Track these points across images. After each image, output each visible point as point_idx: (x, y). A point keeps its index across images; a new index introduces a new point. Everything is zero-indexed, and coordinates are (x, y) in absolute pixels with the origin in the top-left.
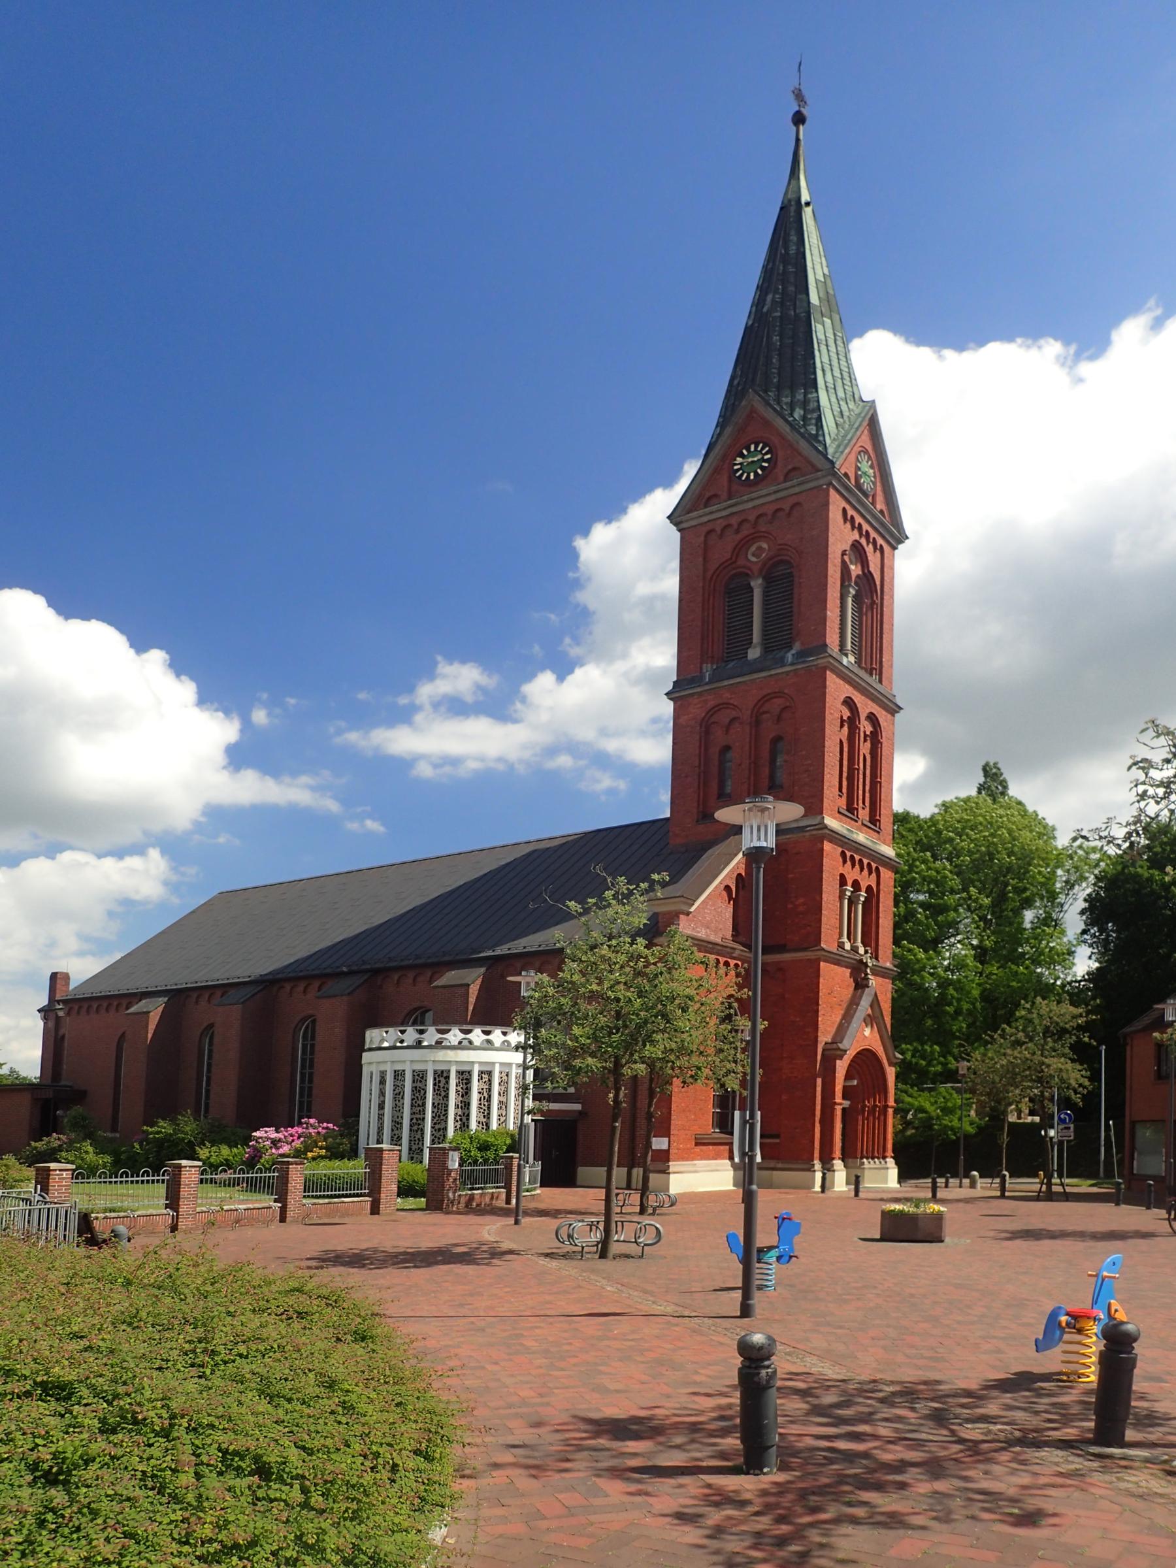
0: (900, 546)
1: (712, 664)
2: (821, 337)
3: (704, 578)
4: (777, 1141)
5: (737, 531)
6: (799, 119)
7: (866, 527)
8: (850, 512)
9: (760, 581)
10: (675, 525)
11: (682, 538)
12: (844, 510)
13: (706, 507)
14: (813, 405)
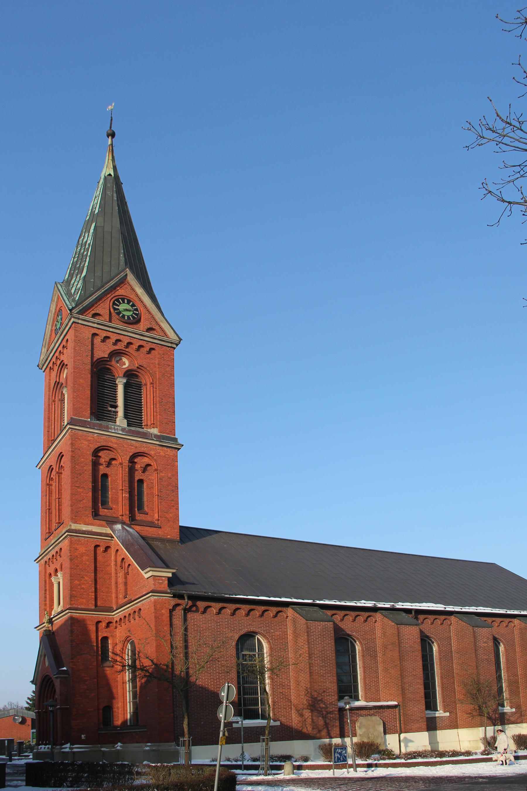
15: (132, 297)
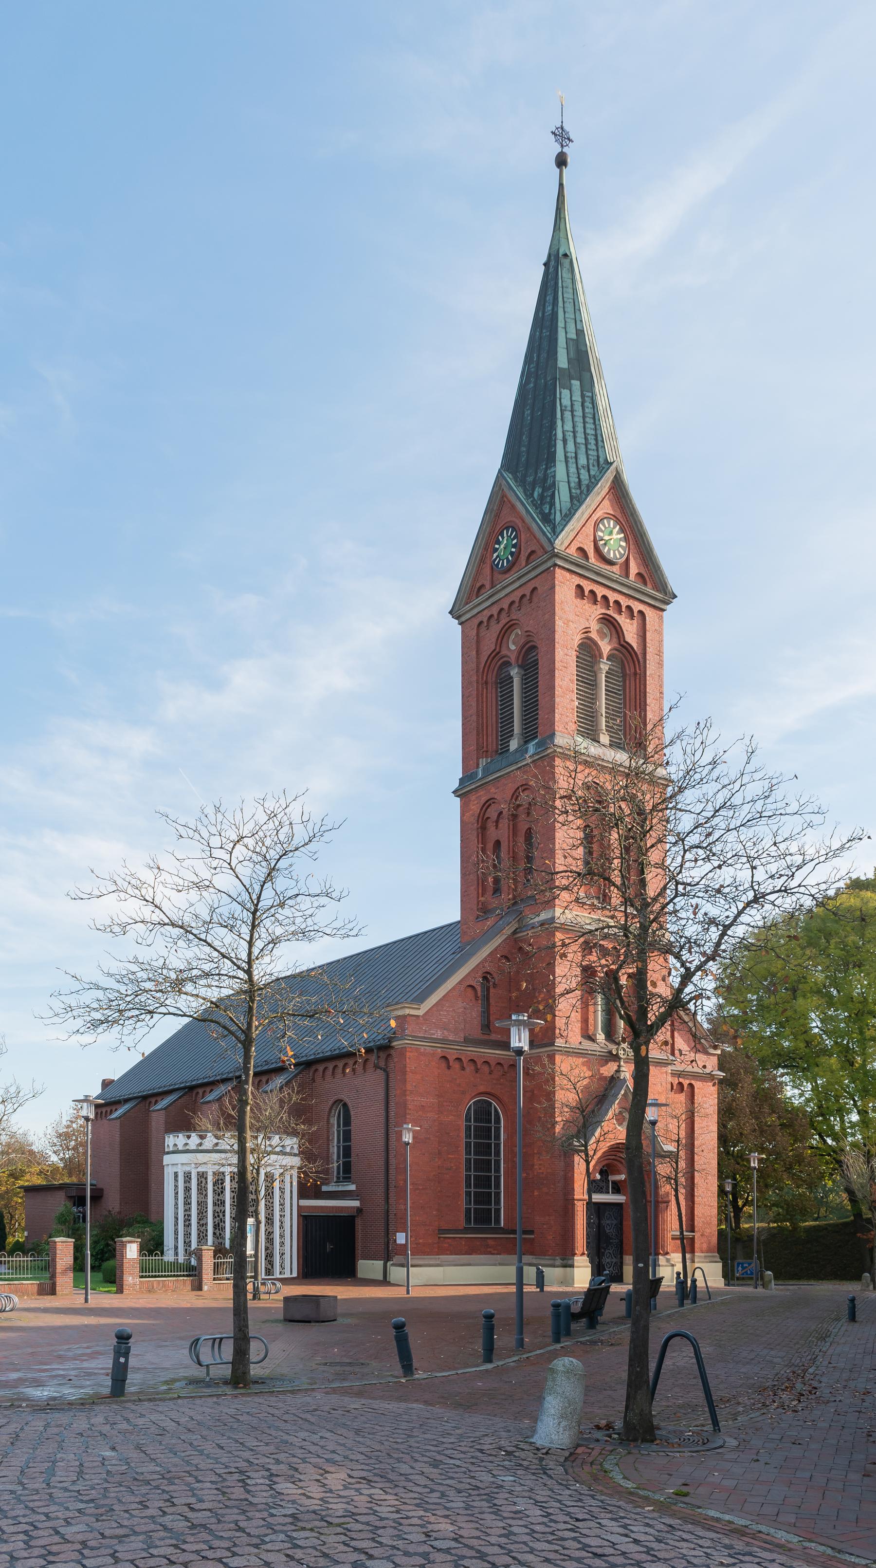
0: (668, 607)
1: (487, 757)
2: (566, 402)
3: (477, 671)
4: (532, 1236)
6: (561, 161)
7: (612, 597)
8: (587, 586)
9: (516, 670)
10: (457, 618)
11: (463, 631)
12: (579, 587)
13: (477, 597)
14: (550, 481)
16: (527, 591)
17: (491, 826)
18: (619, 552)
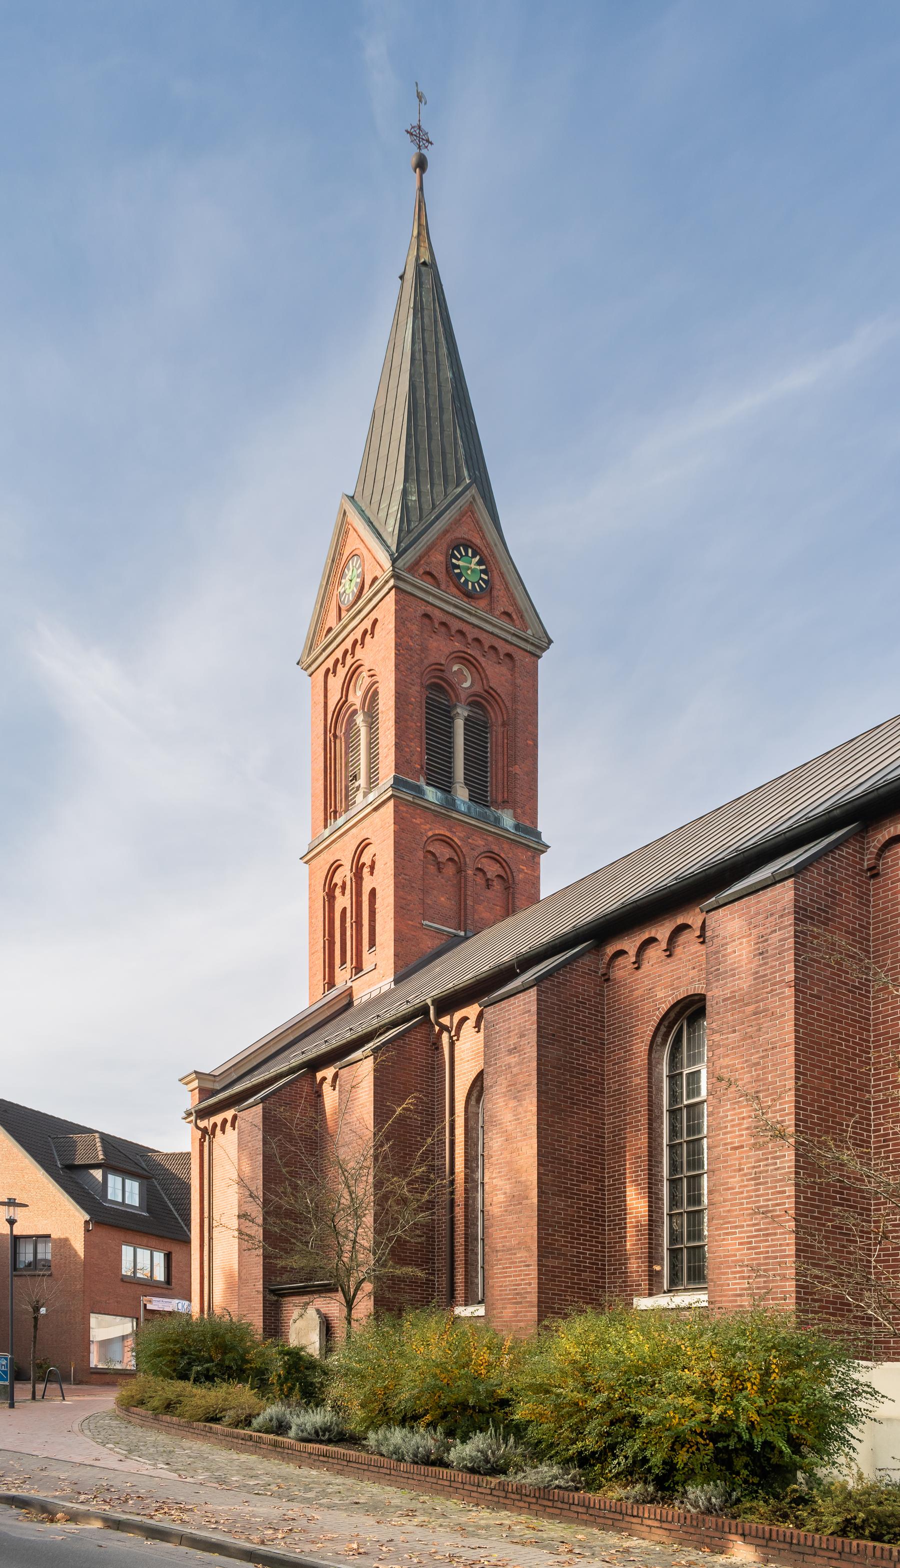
5: (344, 663)
6: (421, 164)
15: (478, 541)
16: (367, 624)
17: (338, 891)
18: (480, 585)
